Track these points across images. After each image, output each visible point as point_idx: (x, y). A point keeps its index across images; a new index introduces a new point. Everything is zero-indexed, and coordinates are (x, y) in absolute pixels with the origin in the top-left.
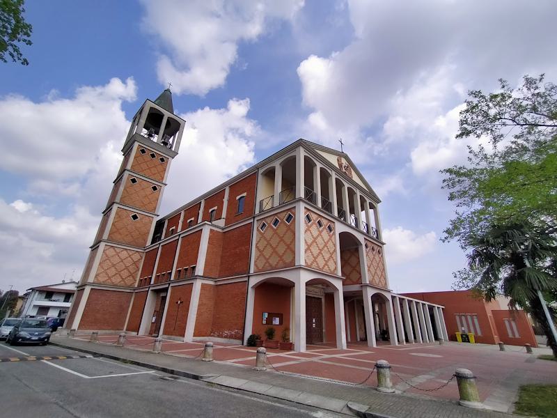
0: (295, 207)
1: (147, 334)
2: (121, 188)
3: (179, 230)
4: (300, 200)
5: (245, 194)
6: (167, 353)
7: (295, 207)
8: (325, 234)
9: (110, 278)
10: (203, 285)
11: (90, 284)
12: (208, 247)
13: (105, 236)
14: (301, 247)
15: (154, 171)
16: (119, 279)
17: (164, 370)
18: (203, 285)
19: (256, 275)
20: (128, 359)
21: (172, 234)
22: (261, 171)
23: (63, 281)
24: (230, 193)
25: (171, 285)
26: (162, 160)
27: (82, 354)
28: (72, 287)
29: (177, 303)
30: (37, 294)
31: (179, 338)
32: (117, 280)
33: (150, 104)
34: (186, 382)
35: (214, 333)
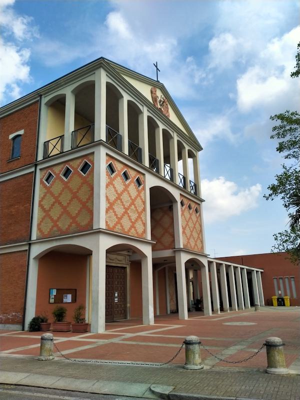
4: (100, 143)
7: (93, 153)
8: (133, 189)
19: (42, 240)
22: (45, 100)
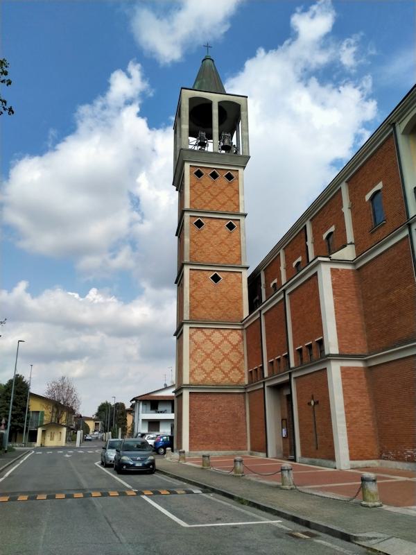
1: (281, 455)
2: (187, 240)
3: (284, 281)
5: (379, 186)
6: (306, 489)
9: (208, 374)
11: (188, 387)
12: (335, 303)
15: (222, 198)
16: (221, 376)
17: (295, 520)
18: (344, 371)
20: (245, 498)
21: (276, 290)
22: (400, 129)
23: (165, 385)
24: (350, 194)
25: (293, 376)
26: (229, 177)
27: (190, 488)
28: (169, 393)
29: (309, 404)
30: (141, 406)
31: (324, 462)
32: (218, 377)
33: (188, 94)
34: (329, 544)
35: (387, 453)
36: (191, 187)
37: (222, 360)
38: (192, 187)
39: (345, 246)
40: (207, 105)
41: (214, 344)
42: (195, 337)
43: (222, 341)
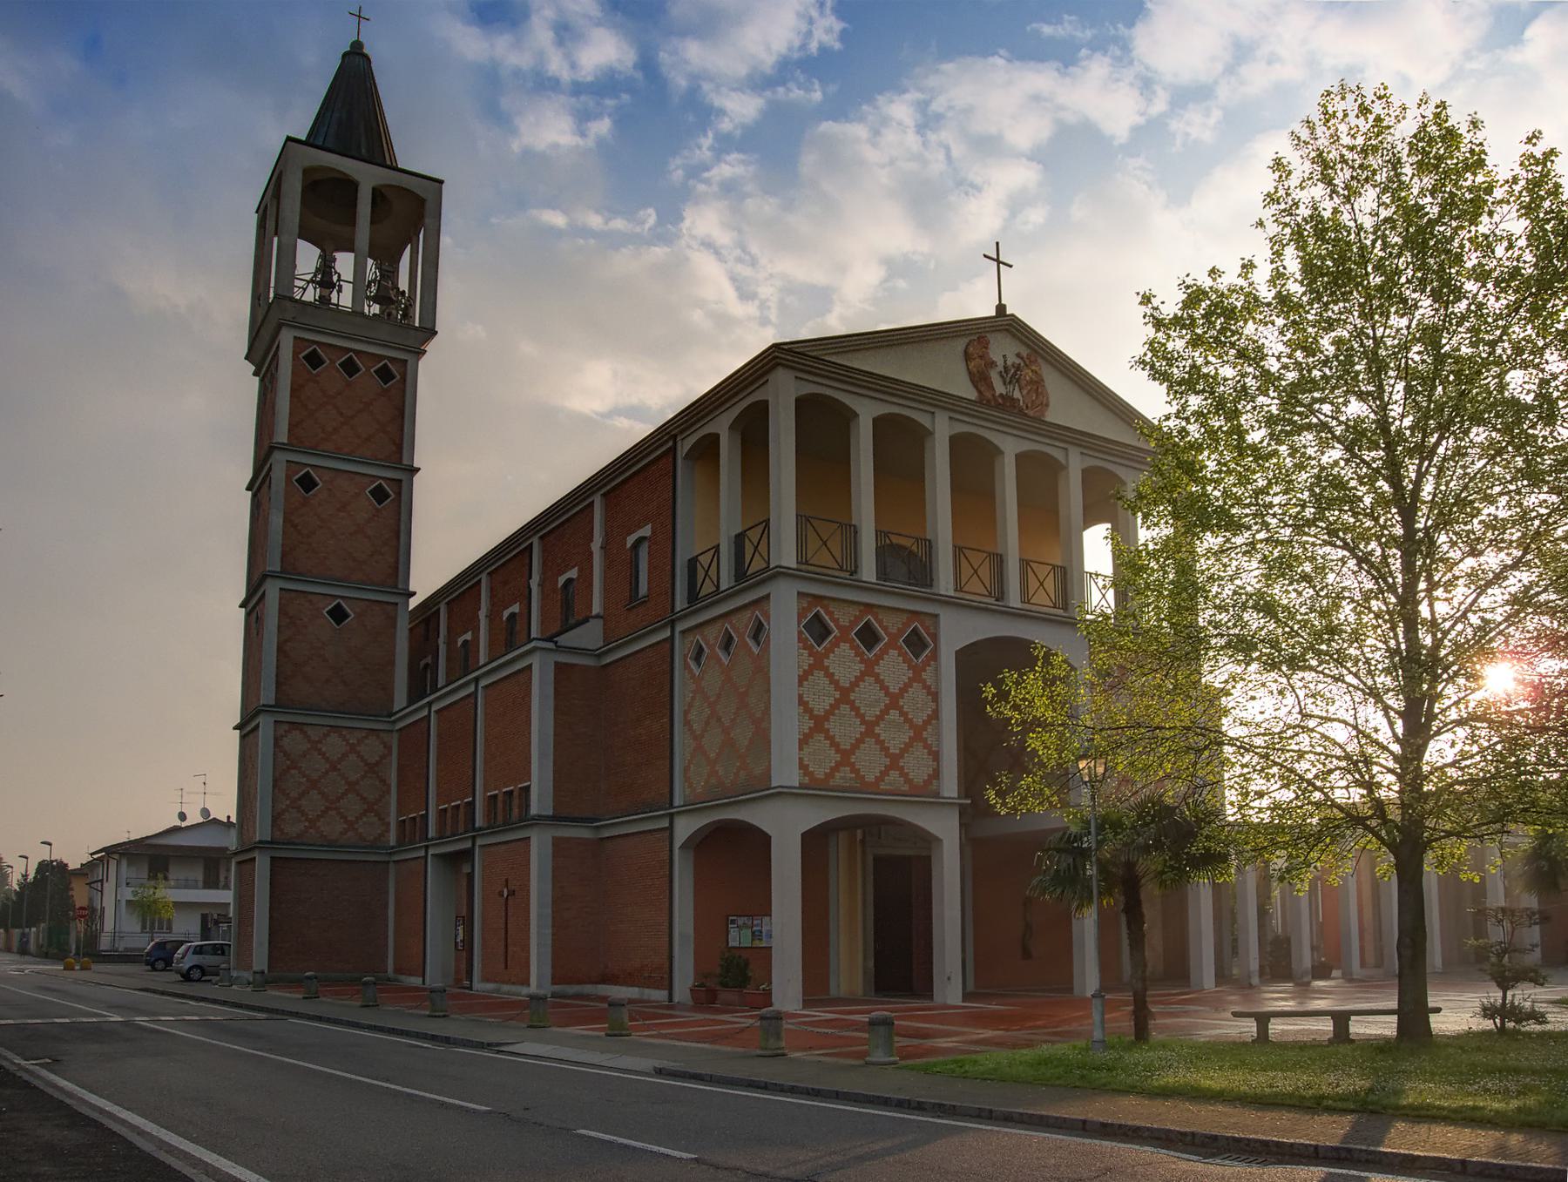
0: (768, 596)
4: (781, 573)
7: (768, 596)
8: (894, 668)
10: (557, 842)
11: (261, 846)
13: (282, 436)
14: (786, 726)
19: (691, 810)
22: (684, 447)
25: (479, 842)
36: (293, 390)
37: (345, 794)
38: (295, 391)
39: (586, 620)
40: (349, 186)
41: (327, 759)
42: (286, 742)
43: (345, 755)
